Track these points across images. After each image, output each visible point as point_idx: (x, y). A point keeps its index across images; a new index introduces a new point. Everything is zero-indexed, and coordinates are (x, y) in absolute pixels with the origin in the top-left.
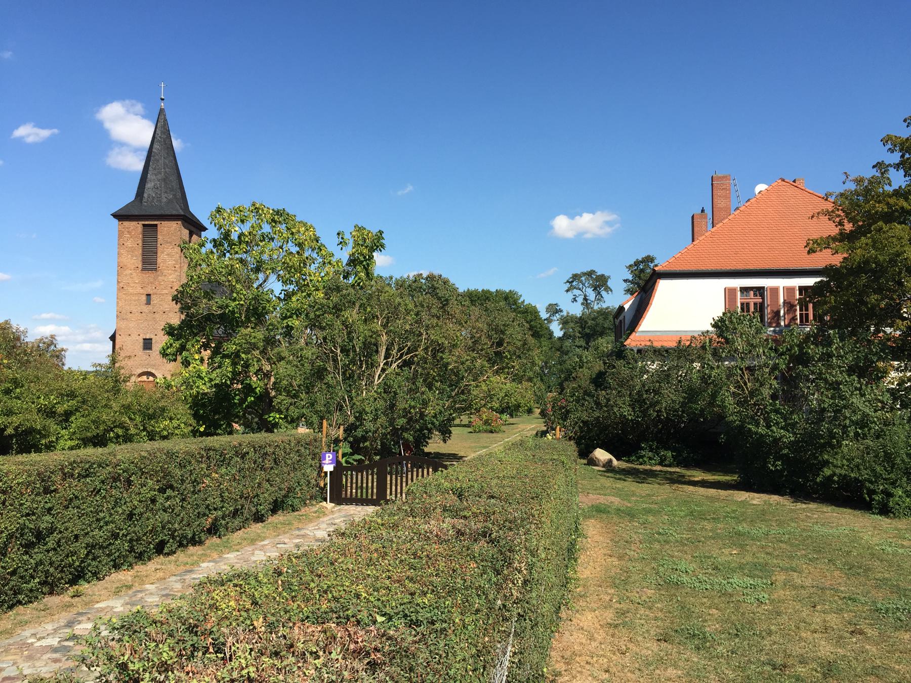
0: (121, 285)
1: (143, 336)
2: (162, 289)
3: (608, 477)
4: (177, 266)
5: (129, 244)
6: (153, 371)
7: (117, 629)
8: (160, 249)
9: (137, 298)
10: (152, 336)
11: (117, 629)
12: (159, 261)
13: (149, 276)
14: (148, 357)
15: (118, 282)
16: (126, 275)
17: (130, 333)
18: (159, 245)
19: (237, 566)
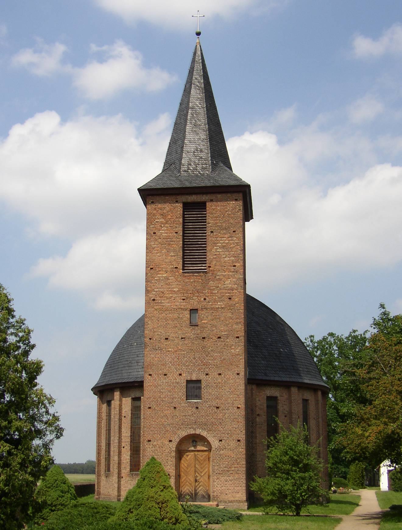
0: (152, 296)
1: (186, 376)
2: (215, 301)
3: (106, 462)
4: (237, 264)
5: (163, 232)
6: (204, 434)
7: (338, 413)
8: (210, 239)
9: (176, 315)
10: (202, 377)
11: (338, 413)
12: (210, 256)
13: (194, 281)
14: (194, 410)
15: (147, 291)
16: (159, 280)
17: (165, 371)
18: (208, 233)
19: (225, 196)
